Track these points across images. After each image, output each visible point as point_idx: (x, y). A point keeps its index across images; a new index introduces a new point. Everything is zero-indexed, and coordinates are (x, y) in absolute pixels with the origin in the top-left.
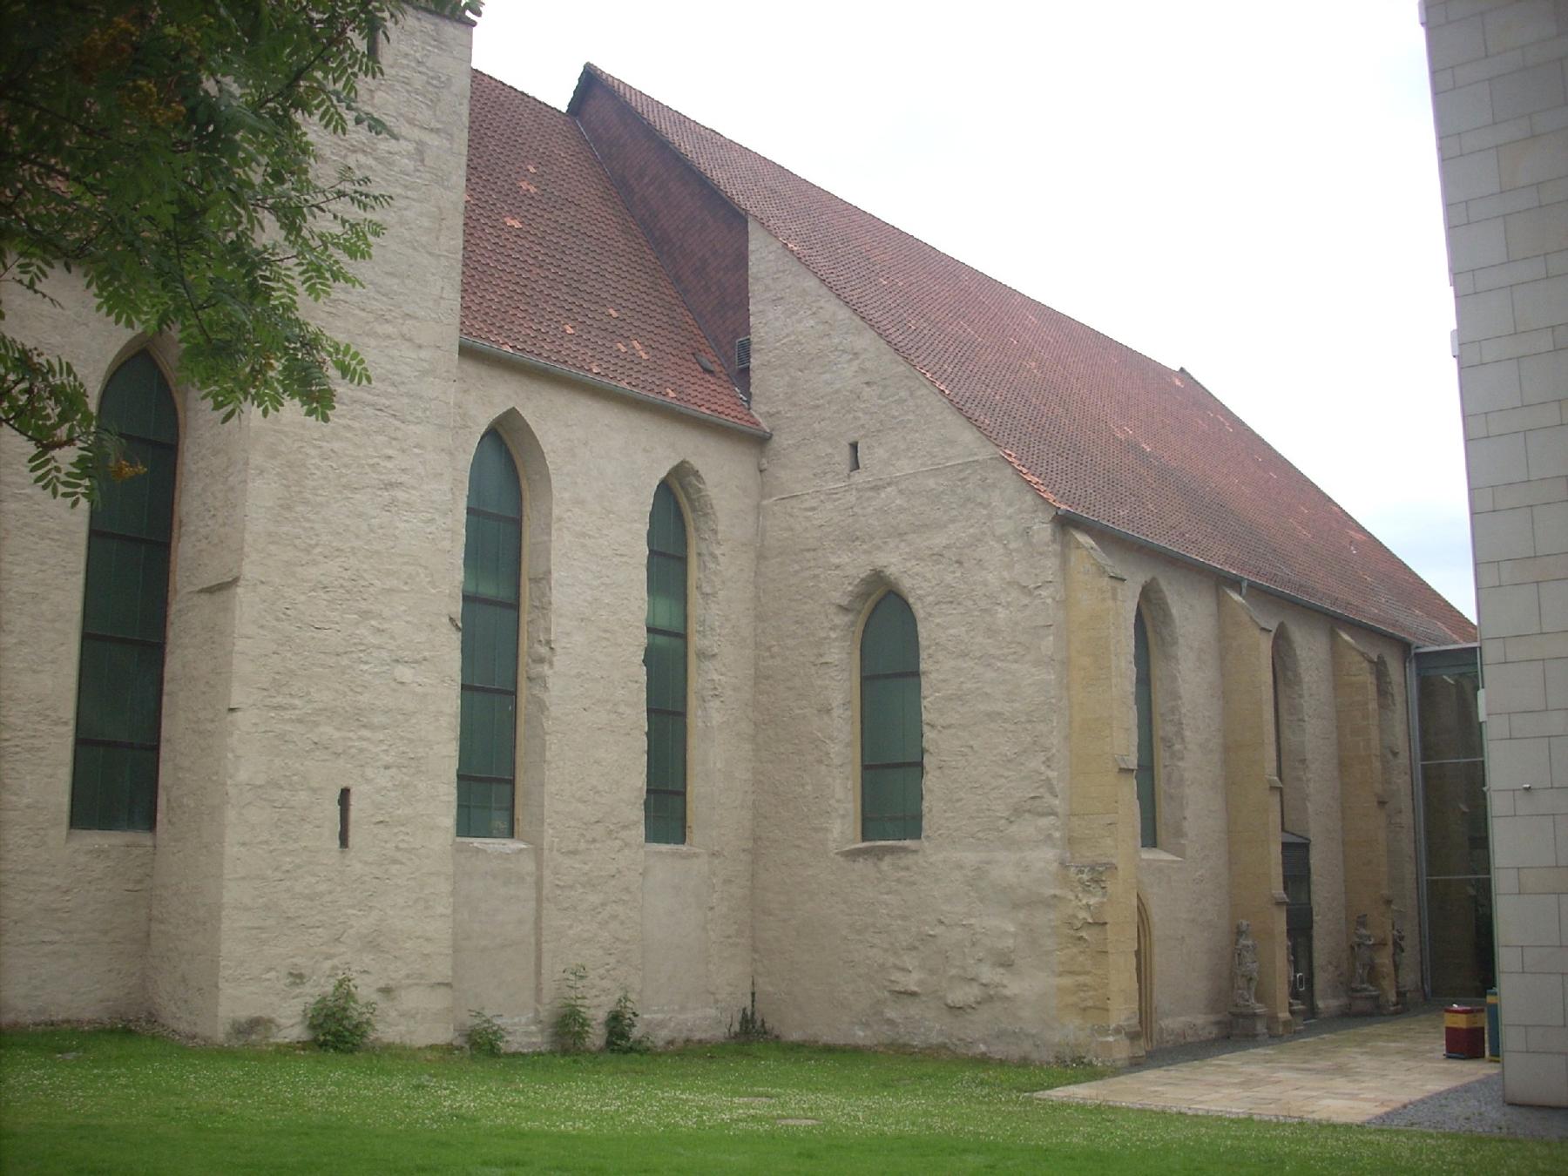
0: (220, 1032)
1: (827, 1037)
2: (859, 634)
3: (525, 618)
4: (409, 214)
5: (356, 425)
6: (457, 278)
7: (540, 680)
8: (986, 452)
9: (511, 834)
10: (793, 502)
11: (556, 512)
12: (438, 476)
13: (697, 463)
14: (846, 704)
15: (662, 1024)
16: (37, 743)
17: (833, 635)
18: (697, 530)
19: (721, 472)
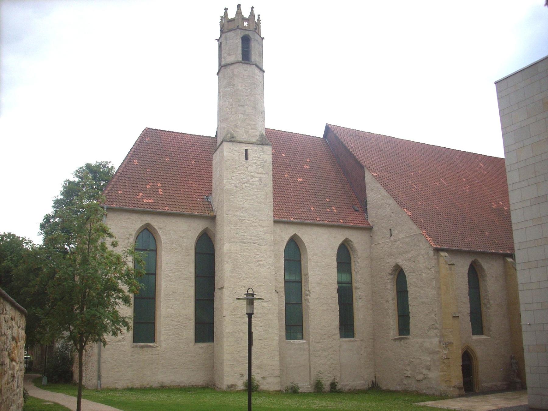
0: (224, 387)
1: (392, 388)
2: (396, 280)
3: (303, 285)
4: (259, 196)
5: (249, 248)
6: (272, 208)
7: (307, 300)
8: (418, 231)
9: (302, 339)
10: (378, 245)
11: (309, 258)
12: (270, 257)
13: (350, 238)
14: (393, 299)
15: (347, 385)
16: (186, 325)
19: (358, 239)
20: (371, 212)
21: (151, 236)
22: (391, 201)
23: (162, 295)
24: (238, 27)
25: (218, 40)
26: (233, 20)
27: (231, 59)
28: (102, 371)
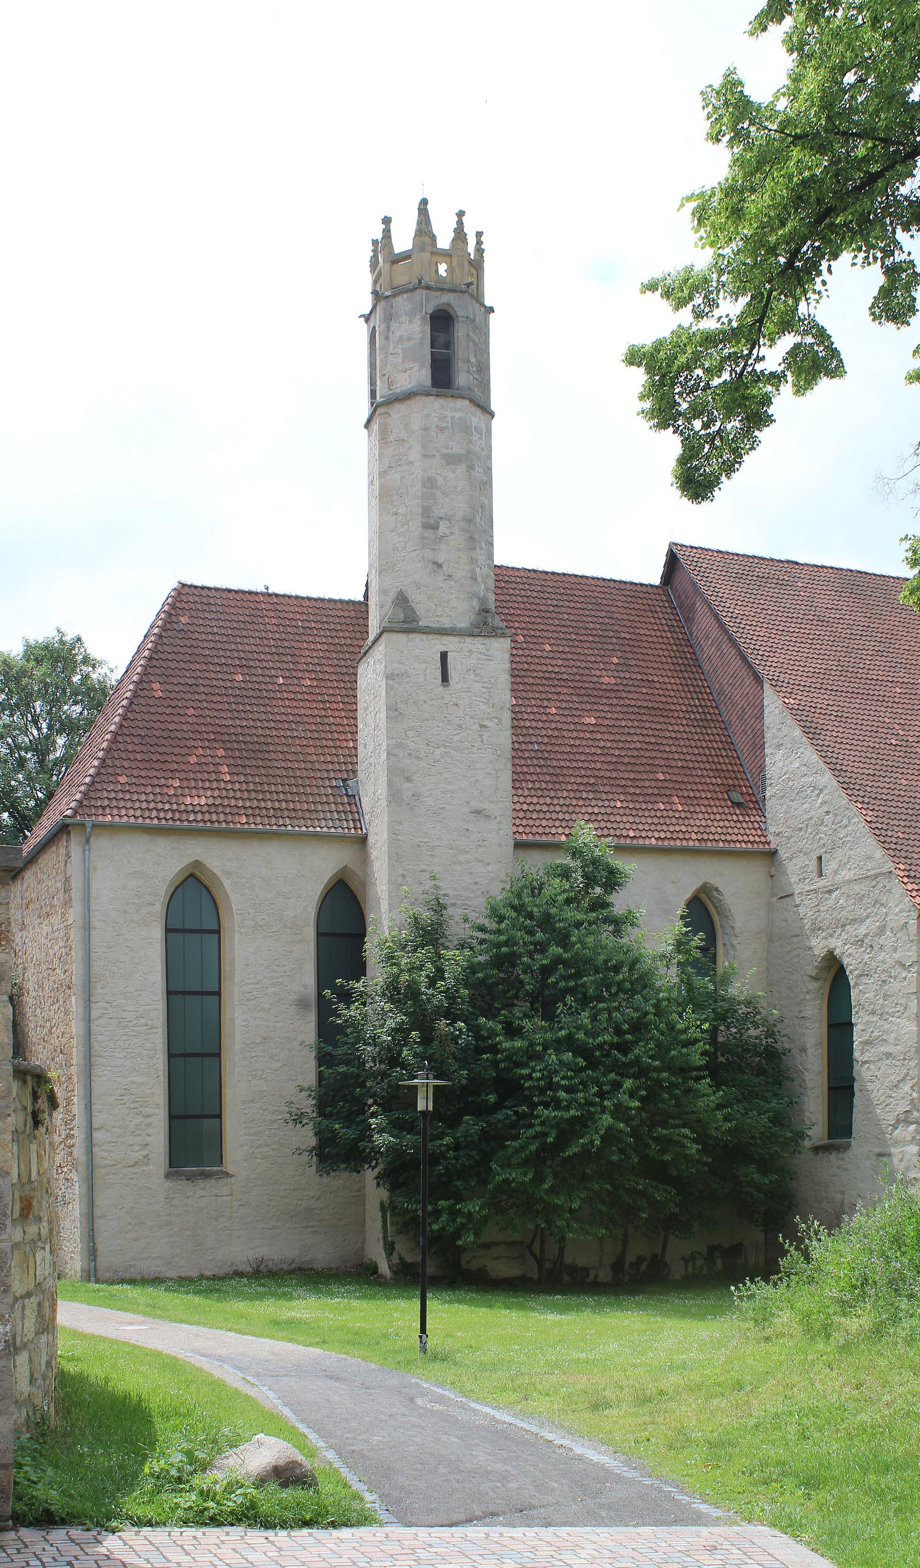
13: (715, 882)
17: (808, 997)
18: (722, 927)
20: (775, 808)
21: (205, 892)
22: (827, 779)
23: (237, 1047)
24: (420, 282)
25: (367, 318)
26: (406, 256)
27: (404, 383)
28: (99, 1239)
